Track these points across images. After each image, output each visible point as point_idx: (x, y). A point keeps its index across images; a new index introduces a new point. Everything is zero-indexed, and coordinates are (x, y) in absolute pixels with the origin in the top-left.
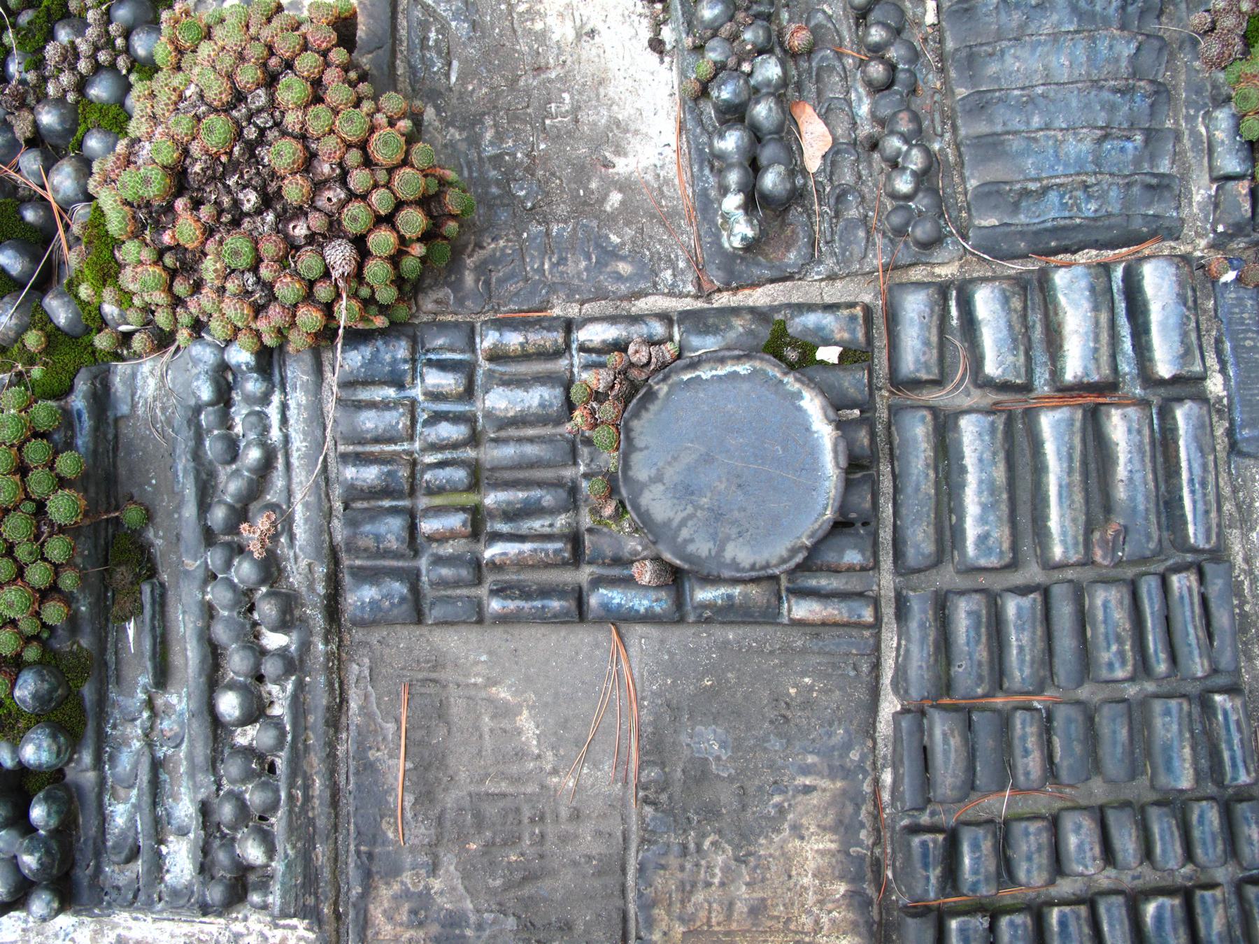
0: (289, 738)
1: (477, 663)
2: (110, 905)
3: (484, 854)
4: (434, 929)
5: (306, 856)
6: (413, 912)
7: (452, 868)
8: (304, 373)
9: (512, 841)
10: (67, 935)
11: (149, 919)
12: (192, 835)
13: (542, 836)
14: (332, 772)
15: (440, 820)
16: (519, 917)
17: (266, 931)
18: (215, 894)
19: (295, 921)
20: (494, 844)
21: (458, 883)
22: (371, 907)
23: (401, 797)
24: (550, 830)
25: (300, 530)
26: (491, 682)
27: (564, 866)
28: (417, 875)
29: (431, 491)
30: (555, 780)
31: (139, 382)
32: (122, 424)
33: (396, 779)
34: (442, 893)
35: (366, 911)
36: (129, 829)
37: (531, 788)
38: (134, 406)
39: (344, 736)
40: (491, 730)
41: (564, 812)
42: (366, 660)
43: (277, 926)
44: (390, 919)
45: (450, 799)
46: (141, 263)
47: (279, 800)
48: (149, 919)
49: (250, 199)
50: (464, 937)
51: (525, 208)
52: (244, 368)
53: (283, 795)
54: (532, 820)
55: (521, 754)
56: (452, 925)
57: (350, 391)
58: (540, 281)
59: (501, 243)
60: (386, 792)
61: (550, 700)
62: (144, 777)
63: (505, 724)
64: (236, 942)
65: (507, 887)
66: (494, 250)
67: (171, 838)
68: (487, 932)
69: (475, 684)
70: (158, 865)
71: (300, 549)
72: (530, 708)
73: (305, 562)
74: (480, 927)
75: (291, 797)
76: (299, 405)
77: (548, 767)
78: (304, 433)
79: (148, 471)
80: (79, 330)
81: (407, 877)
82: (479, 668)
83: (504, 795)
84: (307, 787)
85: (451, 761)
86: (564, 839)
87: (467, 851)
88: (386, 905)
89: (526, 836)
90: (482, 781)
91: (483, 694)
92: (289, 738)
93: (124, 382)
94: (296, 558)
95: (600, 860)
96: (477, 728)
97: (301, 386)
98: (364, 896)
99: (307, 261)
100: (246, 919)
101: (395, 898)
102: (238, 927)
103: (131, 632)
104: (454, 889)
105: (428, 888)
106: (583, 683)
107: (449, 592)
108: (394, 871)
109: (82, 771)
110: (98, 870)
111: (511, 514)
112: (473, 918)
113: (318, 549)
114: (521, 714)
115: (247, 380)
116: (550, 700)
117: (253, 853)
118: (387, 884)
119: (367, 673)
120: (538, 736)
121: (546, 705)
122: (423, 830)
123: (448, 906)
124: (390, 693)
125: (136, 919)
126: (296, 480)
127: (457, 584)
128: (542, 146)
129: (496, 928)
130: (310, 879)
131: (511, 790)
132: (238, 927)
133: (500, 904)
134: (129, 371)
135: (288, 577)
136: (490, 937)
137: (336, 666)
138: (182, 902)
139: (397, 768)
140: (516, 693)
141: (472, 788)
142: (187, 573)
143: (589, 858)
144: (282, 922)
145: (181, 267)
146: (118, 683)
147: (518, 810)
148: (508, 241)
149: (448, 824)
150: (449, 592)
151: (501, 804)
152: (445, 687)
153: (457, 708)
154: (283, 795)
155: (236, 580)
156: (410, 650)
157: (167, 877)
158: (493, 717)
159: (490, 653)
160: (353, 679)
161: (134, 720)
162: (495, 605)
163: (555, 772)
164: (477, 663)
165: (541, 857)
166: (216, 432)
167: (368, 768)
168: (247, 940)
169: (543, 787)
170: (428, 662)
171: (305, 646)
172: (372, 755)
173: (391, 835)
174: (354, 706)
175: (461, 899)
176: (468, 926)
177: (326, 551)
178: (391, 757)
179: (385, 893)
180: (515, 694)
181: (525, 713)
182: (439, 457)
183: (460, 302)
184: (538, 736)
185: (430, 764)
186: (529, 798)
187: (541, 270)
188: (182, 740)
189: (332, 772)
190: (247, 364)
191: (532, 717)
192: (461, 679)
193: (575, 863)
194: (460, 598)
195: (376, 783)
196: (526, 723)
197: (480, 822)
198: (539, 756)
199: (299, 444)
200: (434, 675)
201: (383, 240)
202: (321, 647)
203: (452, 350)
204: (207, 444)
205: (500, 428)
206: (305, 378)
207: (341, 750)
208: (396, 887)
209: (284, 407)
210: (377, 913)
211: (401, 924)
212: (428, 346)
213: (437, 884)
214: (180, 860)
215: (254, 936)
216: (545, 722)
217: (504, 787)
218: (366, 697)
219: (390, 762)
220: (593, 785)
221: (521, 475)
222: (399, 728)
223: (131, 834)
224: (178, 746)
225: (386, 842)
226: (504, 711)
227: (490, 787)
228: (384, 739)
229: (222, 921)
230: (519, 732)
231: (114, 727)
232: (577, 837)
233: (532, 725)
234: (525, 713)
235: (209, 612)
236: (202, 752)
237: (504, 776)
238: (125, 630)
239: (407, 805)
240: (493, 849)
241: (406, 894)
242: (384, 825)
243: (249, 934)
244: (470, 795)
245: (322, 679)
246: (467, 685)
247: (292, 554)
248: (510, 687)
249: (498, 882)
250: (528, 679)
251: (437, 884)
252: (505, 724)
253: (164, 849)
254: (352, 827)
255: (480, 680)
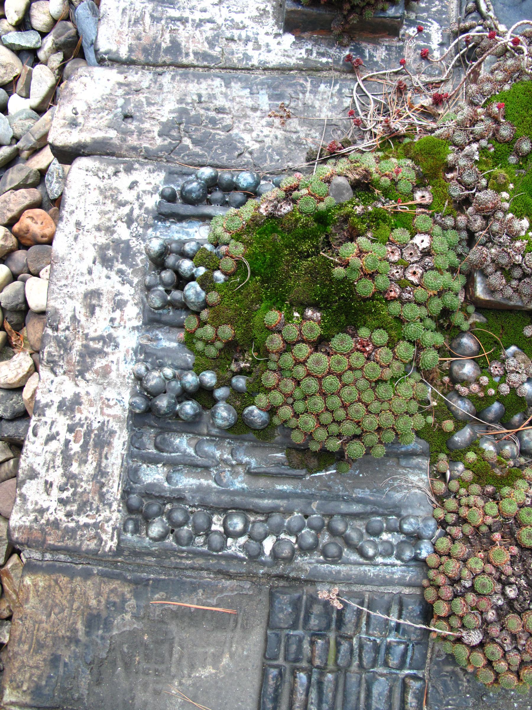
0: (215, 553)
1: (243, 649)
2: (133, 430)
3: (142, 644)
4: (104, 614)
5: (150, 554)
6: (114, 604)
7: (135, 626)
8: (410, 578)
9: (147, 658)
10: (119, 401)
11: (124, 452)
12: (166, 484)
13: (148, 674)
14: (193, 568)
15: (162, 622)
16: (106, 659)
17: (111, 522)
18: (134, 499)
19: (115, 540)
20: (146, 649)
21: (127, 628)
22: (119, 582)
23: (174, 604)
24: (151, 678)
25: (324, 567)
26: (232, 656)
27: (131, 684)
28: (134, 607)
29: (338, 644)
30: (176, 683)
31: (417, 471)
32: (395, 459)
33: (186, 602)
34: (123, 619)
35: (117, 579)
36: (173, 448)
37: (173, 670)
38: (404, 468)
39: (212, 576)
40: (206, 653)
41: (159, 687)
42: (251, 593)
43: (114, 529)
44: (112, 591)
45: (173, 627)
46: (485, 514)
47: (182, 546)
48: (124, 452)
49: (511, 593)
50: (98, 629)
51: (482, 696)
52: (418, 551)
53: (184, 548)
54: (156, 670)
55: (192, 667)
56: (105, 624)
57: (397, 601)
58: (442, 704)
59: (466, 684)
60: (179, 596)
61: (219, 685)
62: (200, 460)
63: (209, 660)
64: (71, 3)
65: (122, 652)
66: (462, 680)
67: (165, 469)
68: (99, 641)
69: (231, 646)
70: (152, 461)
71: (316, 567)
72: (216, 674)
73: (308, 568)
74: (103, 638)
75: (183, 552)
76: (393, 573)
77: (183, 681)
78: (378, 575)
79: (367, 472)
80: (450, 446)
81: (133, 602)
82: (240, 650)
83: (171, 655)
84: (187, 558)
85: (193, 630)
86: (145, 685)
87: (144, 634)
88: (119, 590)
89: (148, 666)
90: (180, 645)
91: (226, 650)
92: (215, 553)
93: (418, 464)
94: (311, 563)
95: (131, 704)
96: (208, 645)
97: (404, 576)
98: (125, 580)
99: (473, 620)
100: (119, 511)
101: (123, 595)
102: (115, 506)
103: (279, 455)
104: (124, 625)
105: (126, 612)
106: (226, 704)
107: (283, 644)
108: (137, 595)
109: (208, 427)
110: (152, 427)
111: (320, 683)
112: (107, 635)
113: (314, 576)
114: (213, 669)
115: (411, 551)
116: (219, 685)
117: (156, 530)
118: (131, 591)
119: (245, 592)
120: (200, 677)
121: (217, 683)
122: (157, 613)
123: (116, 622)
124: (232, 602)
125: (124, 444)
126: (353, 567)
127: (287, 650)
128: (516, 705)
129: (101, 646)
130: (136, 553)
131: (174, 659)
132: (115, 506)
133: (114, 649)
134: (424, 467)
135: (301, 557)
136: (97, 643)
137: (250, 576)
138: (131, 477)
139: (191, 604)
140: (225, 668)
141: (177, 639)
142: (310, 504)
143: (133, 699)
144: (115, 533)
145: (481, 539)
146: (253, 446)
147: (163, 663)
148: (466, 687)
149: (159, 626)
150: (283, 644)
151: (167, 655)
152: (232, 630)
153: (220, 635)
154: (184, 548)
155: (303, 532)
156: (254, 616)
157: (145, 466)
158: (213, 654)
159: (247, 656)
160: (242, 584)
161: (232, 456)
162: (274, 672)
163: (181, 684)
164: (243, 649)
165: (137, 673)
166: (385, 525)
167: (194, 588)
168: (108, 511)
169: (174, 677)
170: (247, 624)
171: (264, 564)
172: (200, 592)
173: (157, 596)
174: (227, 583)
175: (118, 629)
176: (104, 632)
177: (312, 579)
178: (198, 600)
179: (126, 590)
180: (224, 667)
181: (214, 671)
182: (356, 647)
183: (437, 663)
184: (200, 677)
185: (192, 620)
186: (168, 669)
187: (448, 704)
188: (218, 484)
189: (193, 568)
190: (420, 554)
191: (211, 675)
192: (235, 639)
193: (131, 690)
194: (279, 650)
195: (185, 591)
196: (210, 670)
197: (158, 643)
198: (190, 677)
199: (371, 571)
200: (239, 626)
201: (479, 659)
202: (261, 571)
203: (411, 659)
204: (379, 518)
205: (367, 681)
206: (408, 578)
207: (204, 573)
208: (128, 596)
209: (393, 565)
210: (115, 584)
211: (108, 597)
212: (416, 646)
213: (128, 617)
214: (153, 475)
215: (109, 515)
216: (208, 682)
217: (176, 656)
218: (232, 591)
219: (195, 600)
220: (171, 703)
221: (340, 689)
222: (213, 606)
223: (171, 449)
224: (215, 481)
225: (153, 593)
226: (216, 659)
227: (177, 648)
228: (208, 598)
229: (119, 497)
230: (204, 667)
231: (229, 443)
232: (145, 692)
233: (207, 674)
234: (214, 671)
235: (289, 512)
236: (213, 499)
237: (181, 657)
238: (281, 451)
239: (172, 607)
240: (143, 648)
241: (124, 601)
242: (162, 593)
243: (111, 512)
244: (174, 638)
245: (244, 571)
246: (231, 643)
247: (313, 561)
248: (228, 664)
249: (126, 650)
250: (231, 675)
251: (128, 617)
252: (209, 660)
253: (160, 465)
254: (163, 577)
255: (234, 649)
